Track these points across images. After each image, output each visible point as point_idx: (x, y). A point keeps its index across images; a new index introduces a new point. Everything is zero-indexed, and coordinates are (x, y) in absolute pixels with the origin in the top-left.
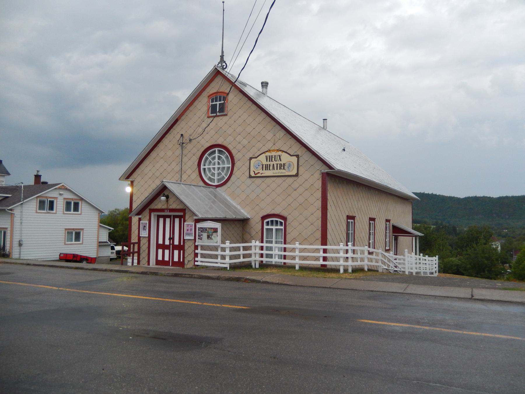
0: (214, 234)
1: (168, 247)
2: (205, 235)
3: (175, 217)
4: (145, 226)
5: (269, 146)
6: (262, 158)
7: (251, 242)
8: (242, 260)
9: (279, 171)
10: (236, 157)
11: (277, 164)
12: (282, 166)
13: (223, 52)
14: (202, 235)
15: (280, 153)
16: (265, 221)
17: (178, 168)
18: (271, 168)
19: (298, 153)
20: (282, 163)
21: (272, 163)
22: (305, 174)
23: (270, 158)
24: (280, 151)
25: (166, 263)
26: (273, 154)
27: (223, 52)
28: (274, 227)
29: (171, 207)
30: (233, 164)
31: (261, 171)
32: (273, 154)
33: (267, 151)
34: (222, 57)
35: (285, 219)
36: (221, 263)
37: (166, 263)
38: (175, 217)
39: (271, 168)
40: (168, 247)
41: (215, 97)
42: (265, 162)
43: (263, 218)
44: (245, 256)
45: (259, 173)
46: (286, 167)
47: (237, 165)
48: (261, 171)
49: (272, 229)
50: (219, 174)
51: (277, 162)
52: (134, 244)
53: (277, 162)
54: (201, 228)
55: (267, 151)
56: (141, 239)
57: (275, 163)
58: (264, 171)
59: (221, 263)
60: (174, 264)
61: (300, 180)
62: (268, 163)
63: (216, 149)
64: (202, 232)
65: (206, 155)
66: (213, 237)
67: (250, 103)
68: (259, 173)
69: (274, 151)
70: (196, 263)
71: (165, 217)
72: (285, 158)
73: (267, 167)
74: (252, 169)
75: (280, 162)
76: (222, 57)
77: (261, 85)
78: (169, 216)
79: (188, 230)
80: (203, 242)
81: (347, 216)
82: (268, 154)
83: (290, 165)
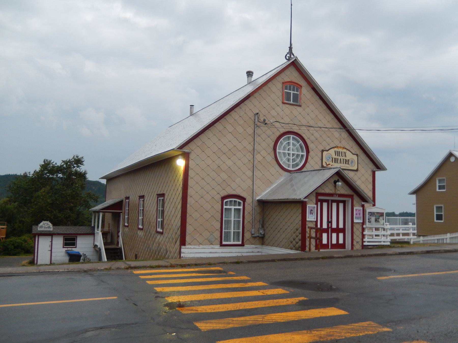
0: (381, 218)
1: (334, 230)
2: (373, 219)
3: (333, 201)
4: (311, 210)
5: (337, 143)
6: (332, 152)
7: (408, 225)
8: (401, 237)
9: (344, 165)
10: (311, 146)
11: (343, 159)
12: (347, 162)
13: (291, 44)
14: (370, 218)
15: (345, 150)
16: (225, 201)
17: (250, 148)
18: (339, 161)
19: (358, 153)
20: (347, 158)
21: (339, 158)
22: (361, 170)
23: (337, 153)
24: (345, 148)
25: (326, 246)
26: (340, 150)
27: (291, 44)
28: (233, 207)
29: (338, 192)
30: (308, 152)
31: (331, 163)
32: (340, 150)
33: (335, 147)
34: (291, 48)
35: (244, 199)
36: (368, 242)
37: (326, 246)
38: (333, 201)
39: (339, 161)
40: (334, 230)
41: (288, 85)
42: (334, 156)
43: (223, 198)
44: (404, 234)
45: (329, 164)
46: (350, 163)
47: (311, 153)
48: (331, 163)
49: (231, 209)
50: (294, 161)
51: (343, 158)
52: (311, 228)
53: (343, 158)
54: (370, 212)
55: (335, 147)
56: (354, 224)
57: (342, 158)
58: (333, 164)
59: (368, 242)
60: (333, 246)
61: (358, 173)
62: (337, 157)
63: (292, 136)
64: (370, 216)
65: (301, 142)
66: (380, 220)
67: (261, 91)
68: (329, 164)
69: (340, 147)
70: (365, 244)
71: (338, 202)
72: (349, 156)
73: (336, 161)
74: (324, 160)
75: (345, 158)
76: (291, 48)
77: (246, 75)
78: (327, 201)
79: (357, 214)
80: (371, 225)
81: (158, 195)
82: (336, 149)
83: (352, 162)
